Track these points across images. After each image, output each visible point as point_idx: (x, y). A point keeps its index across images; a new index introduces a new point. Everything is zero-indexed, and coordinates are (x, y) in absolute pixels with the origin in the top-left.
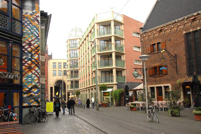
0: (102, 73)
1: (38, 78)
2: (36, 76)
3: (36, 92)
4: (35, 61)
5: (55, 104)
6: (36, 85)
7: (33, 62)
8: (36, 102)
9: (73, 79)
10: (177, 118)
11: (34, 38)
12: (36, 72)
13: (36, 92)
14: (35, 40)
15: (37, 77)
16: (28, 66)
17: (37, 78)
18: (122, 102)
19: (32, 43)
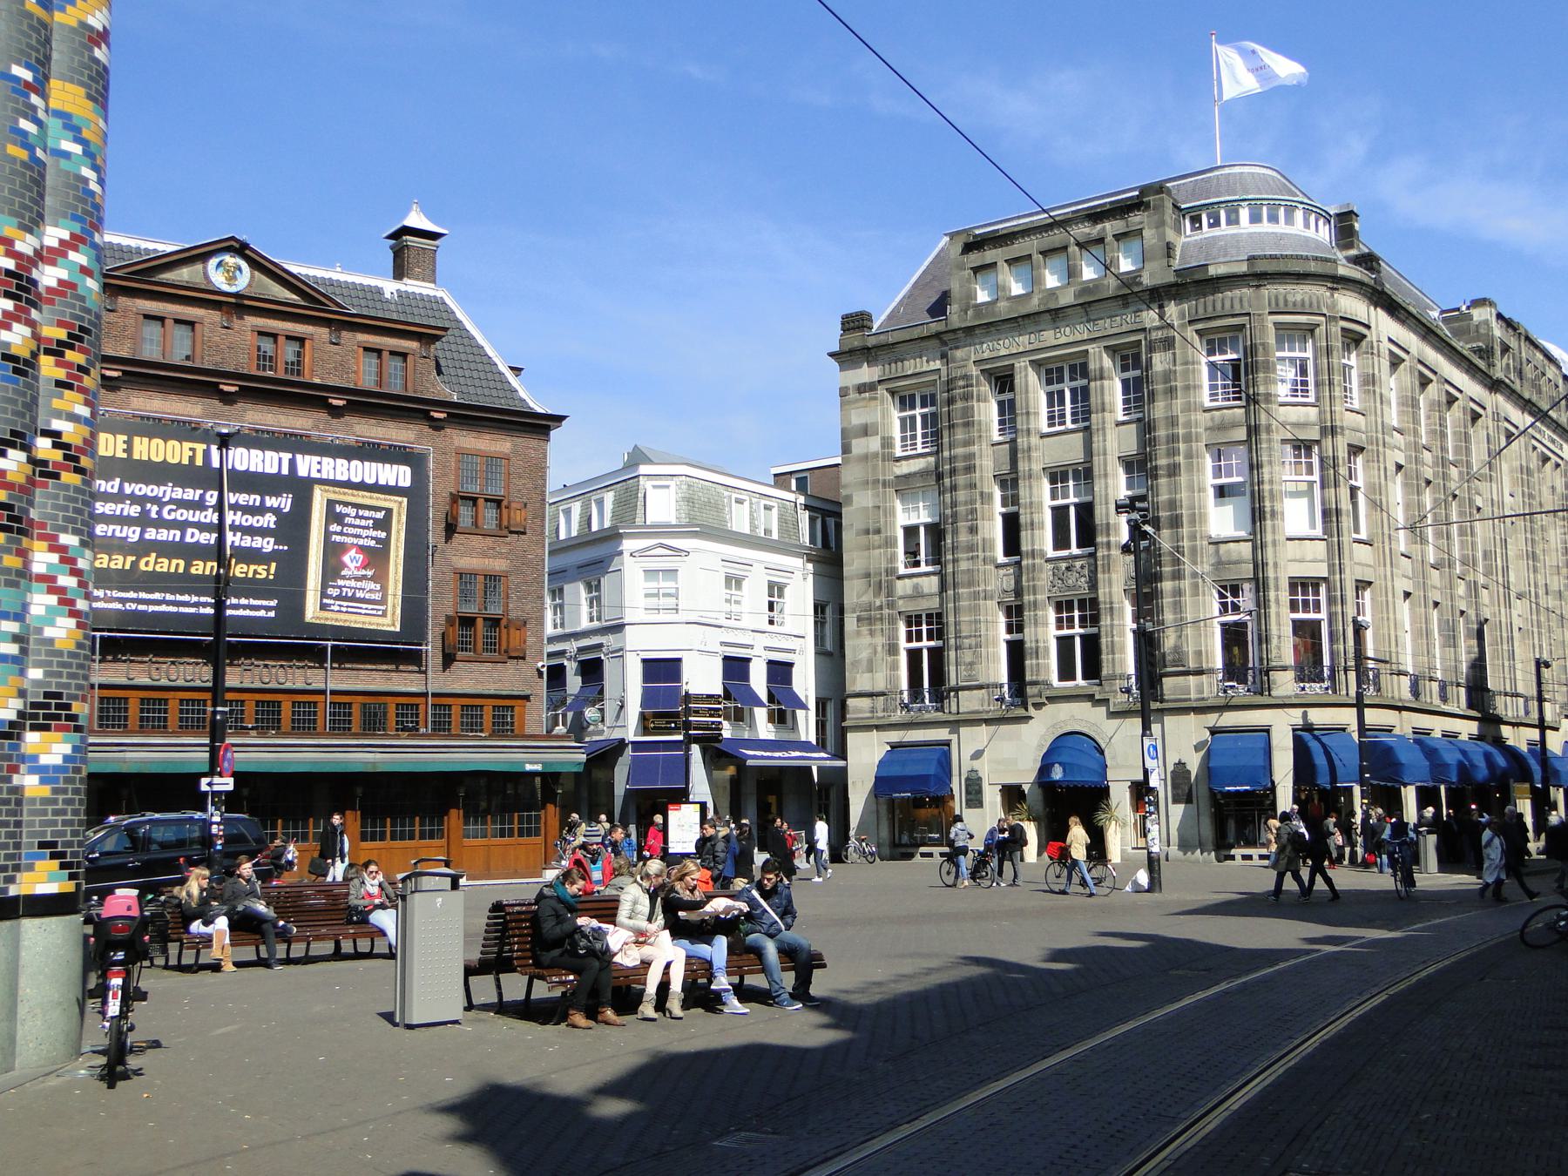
0: (1260, 762)
1: (79, 626)
2: (61, 602)
3: (58, 760)
4: (58, 455)
5: (1176, 285)
6: (73, 286)
7: (44, 463)
8: (56, 863)
9: (1127, 375)
10: (299, 967)
11: (66, 235)
12: (71, 554)
13: (58, 760)
14: (72, 255)
15: (74, 614)
16: (45, 801)
17: (72, 622)
18: (1189, 1145)
19: (48, 276)
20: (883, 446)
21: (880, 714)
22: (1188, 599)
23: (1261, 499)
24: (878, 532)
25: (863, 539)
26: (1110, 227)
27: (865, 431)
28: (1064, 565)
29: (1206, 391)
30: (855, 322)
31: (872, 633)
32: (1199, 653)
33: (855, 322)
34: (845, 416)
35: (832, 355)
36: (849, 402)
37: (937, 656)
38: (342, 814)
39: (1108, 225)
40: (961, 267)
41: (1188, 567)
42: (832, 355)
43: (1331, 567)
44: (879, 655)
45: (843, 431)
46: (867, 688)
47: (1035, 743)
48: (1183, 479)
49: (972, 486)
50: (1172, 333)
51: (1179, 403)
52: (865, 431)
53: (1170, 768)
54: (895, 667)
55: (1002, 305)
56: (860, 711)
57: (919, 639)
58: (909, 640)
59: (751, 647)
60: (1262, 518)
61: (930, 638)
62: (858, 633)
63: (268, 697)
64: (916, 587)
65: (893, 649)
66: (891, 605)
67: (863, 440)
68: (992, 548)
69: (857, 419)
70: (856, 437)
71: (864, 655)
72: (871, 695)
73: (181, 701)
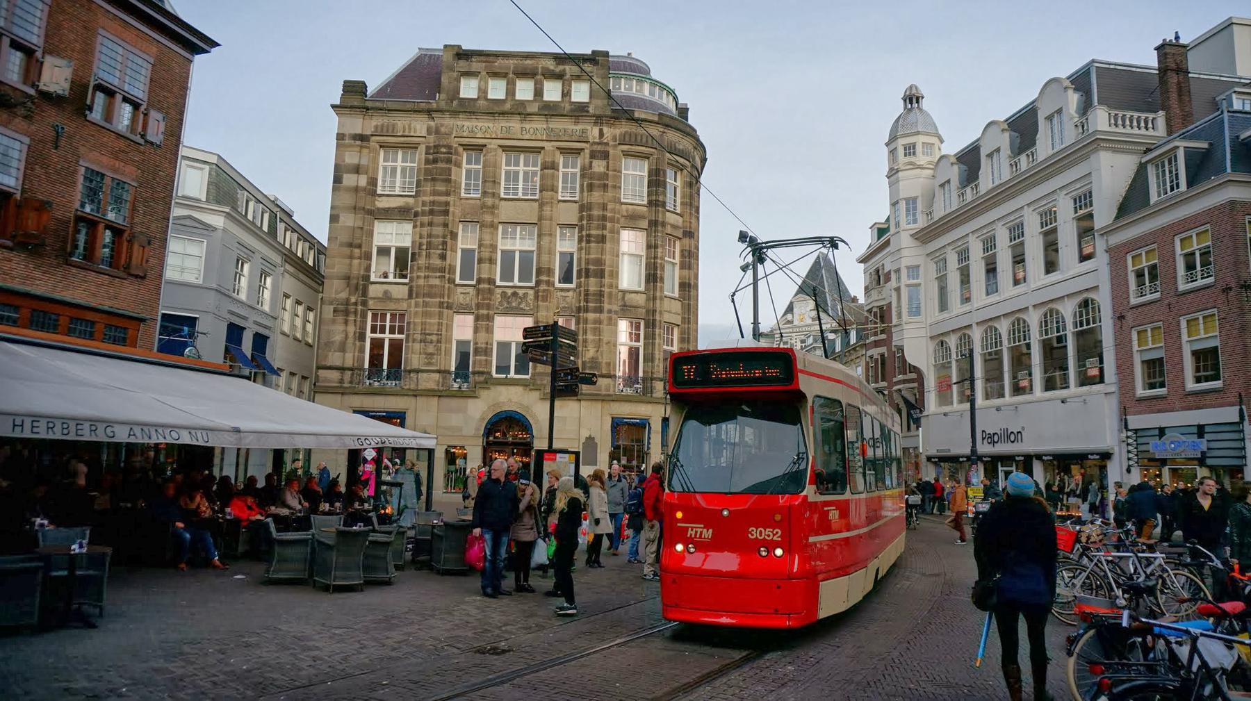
20: (368, 183)
21: (346, 385)
22: (604, 327)
23: (655, 269)
24: (360, 246)
25: (347, 251)
26: (570, 69)
27: (357, 170)
28: (509, 292)
29: (502, 190)
30: (354, 89)
31: (346, 322)
32: (609, 364)
33: (354, 89)
34: (338, 156)
35: (333, 106)
36: (344, 146)
37: (396, 347)
38: (1186, 538)
39: (567, 68)
40: (452, 69)
41: (606, 306)
42: (333, 106)
43: (683, 318)
44: (350, 340)
45: (336, 166)
46: (338, 363)
47: (478, 416)
48: (608, 245)
49: (446, 225)
50: (607, 148)
51: (610, 194)
52: (357, 170)
53: (583, 440)
54: (362, 350)
55: (481, 102)
56: (330, 381)
57: (383, 331)
58: (374, 331)
59: (245, 318)
60: (655, 281)
61: (392, 331)
62: (334, 322)
63: (115, 321)
64: (386, 292)
65: (362, 337)
66: (364, 303)
67: (354, 176)
68: (454, 273)
69: (351, 158)
70: (349, 172)
71: (338, 338)
72: (342, 369)
73: (71, 318)
